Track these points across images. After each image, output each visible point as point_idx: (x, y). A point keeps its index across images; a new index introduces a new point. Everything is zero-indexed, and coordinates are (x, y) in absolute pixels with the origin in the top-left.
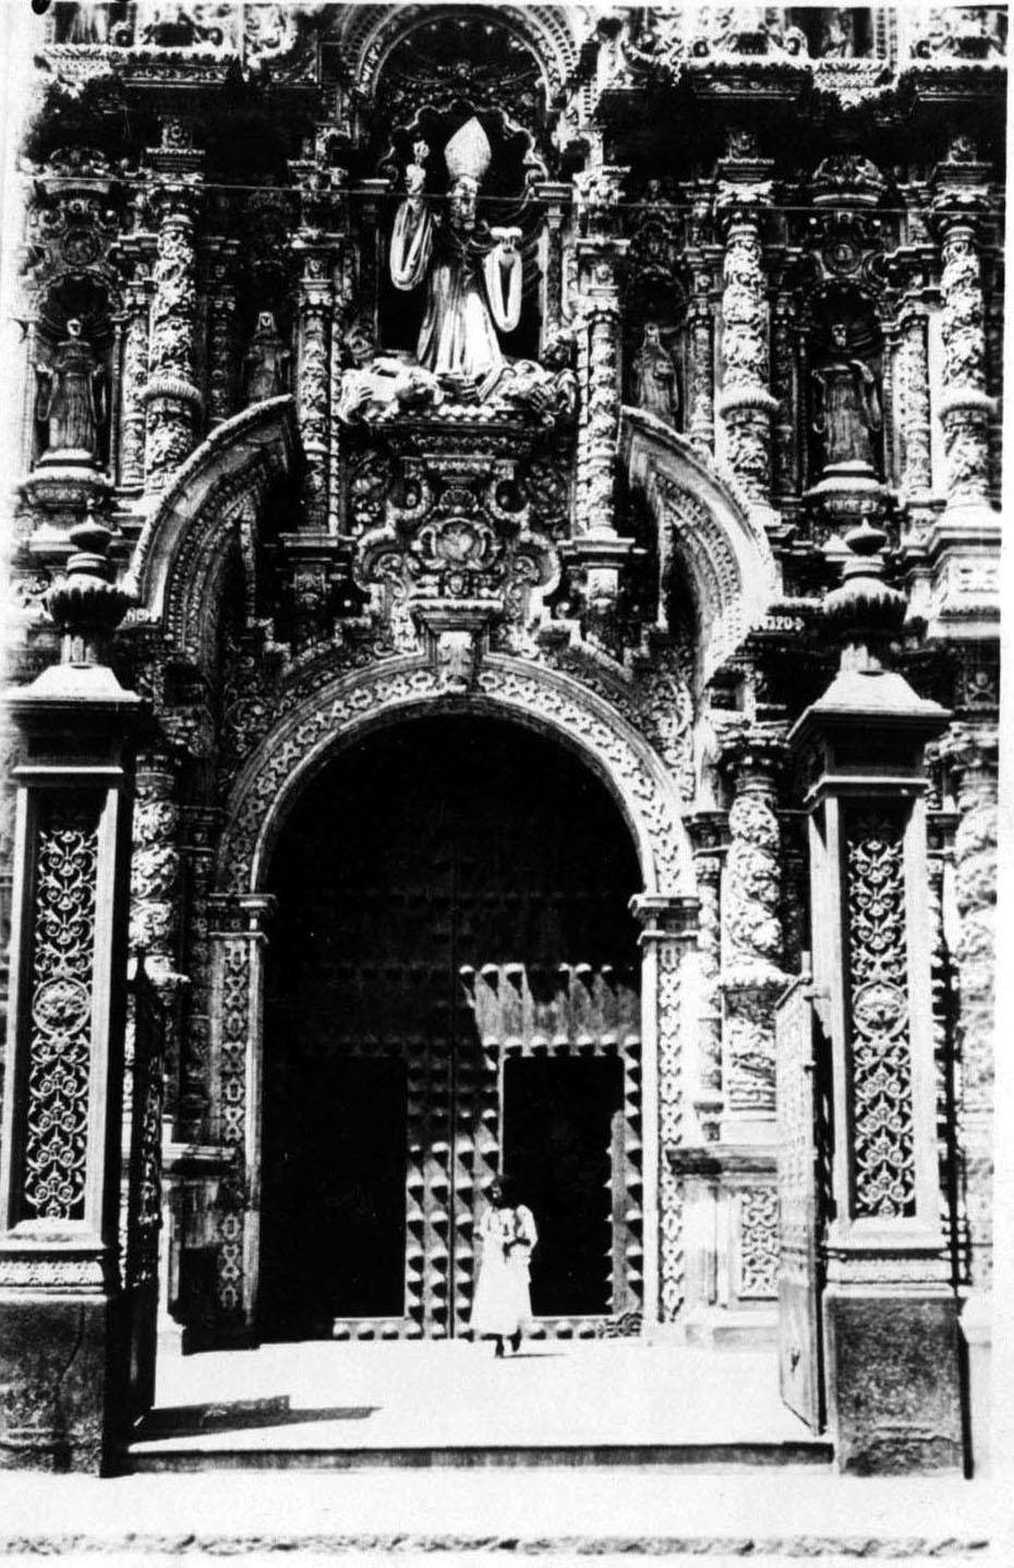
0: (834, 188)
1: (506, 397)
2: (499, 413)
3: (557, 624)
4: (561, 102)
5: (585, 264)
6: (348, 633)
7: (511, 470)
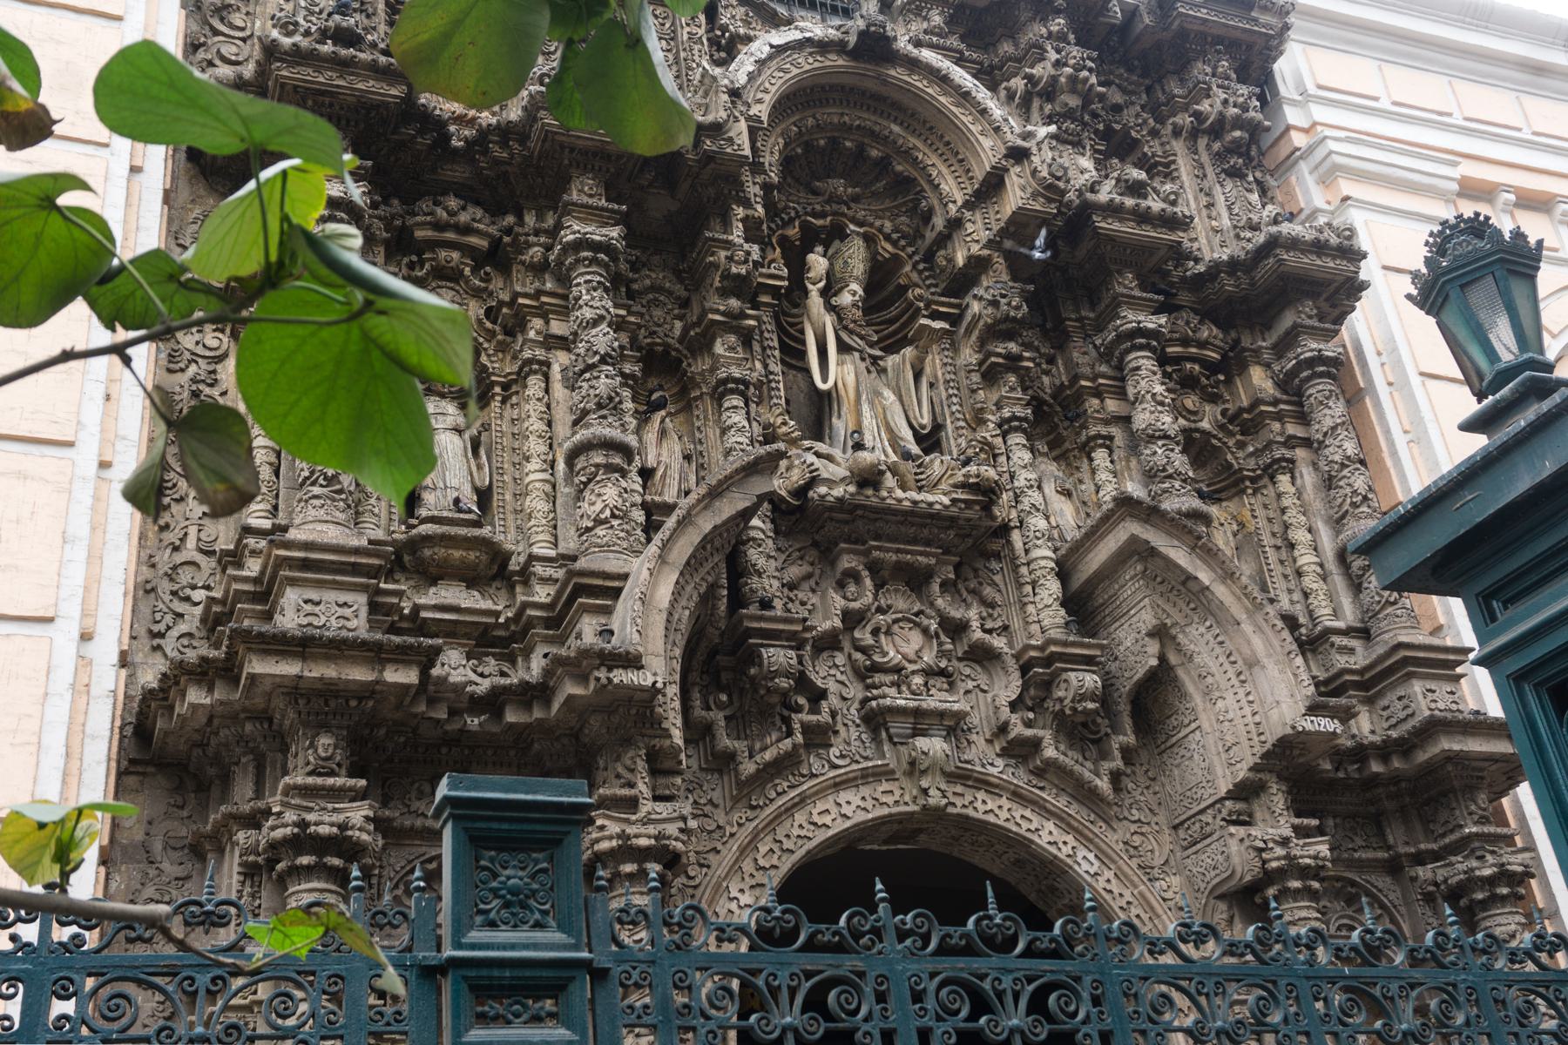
0: (1185, 342)
1: (964, 486)
2: (954, 501)
3: (1029, 732)
4: (956, 224)
5: (990, 376)
6: (807, 729)
7: (951, 568)
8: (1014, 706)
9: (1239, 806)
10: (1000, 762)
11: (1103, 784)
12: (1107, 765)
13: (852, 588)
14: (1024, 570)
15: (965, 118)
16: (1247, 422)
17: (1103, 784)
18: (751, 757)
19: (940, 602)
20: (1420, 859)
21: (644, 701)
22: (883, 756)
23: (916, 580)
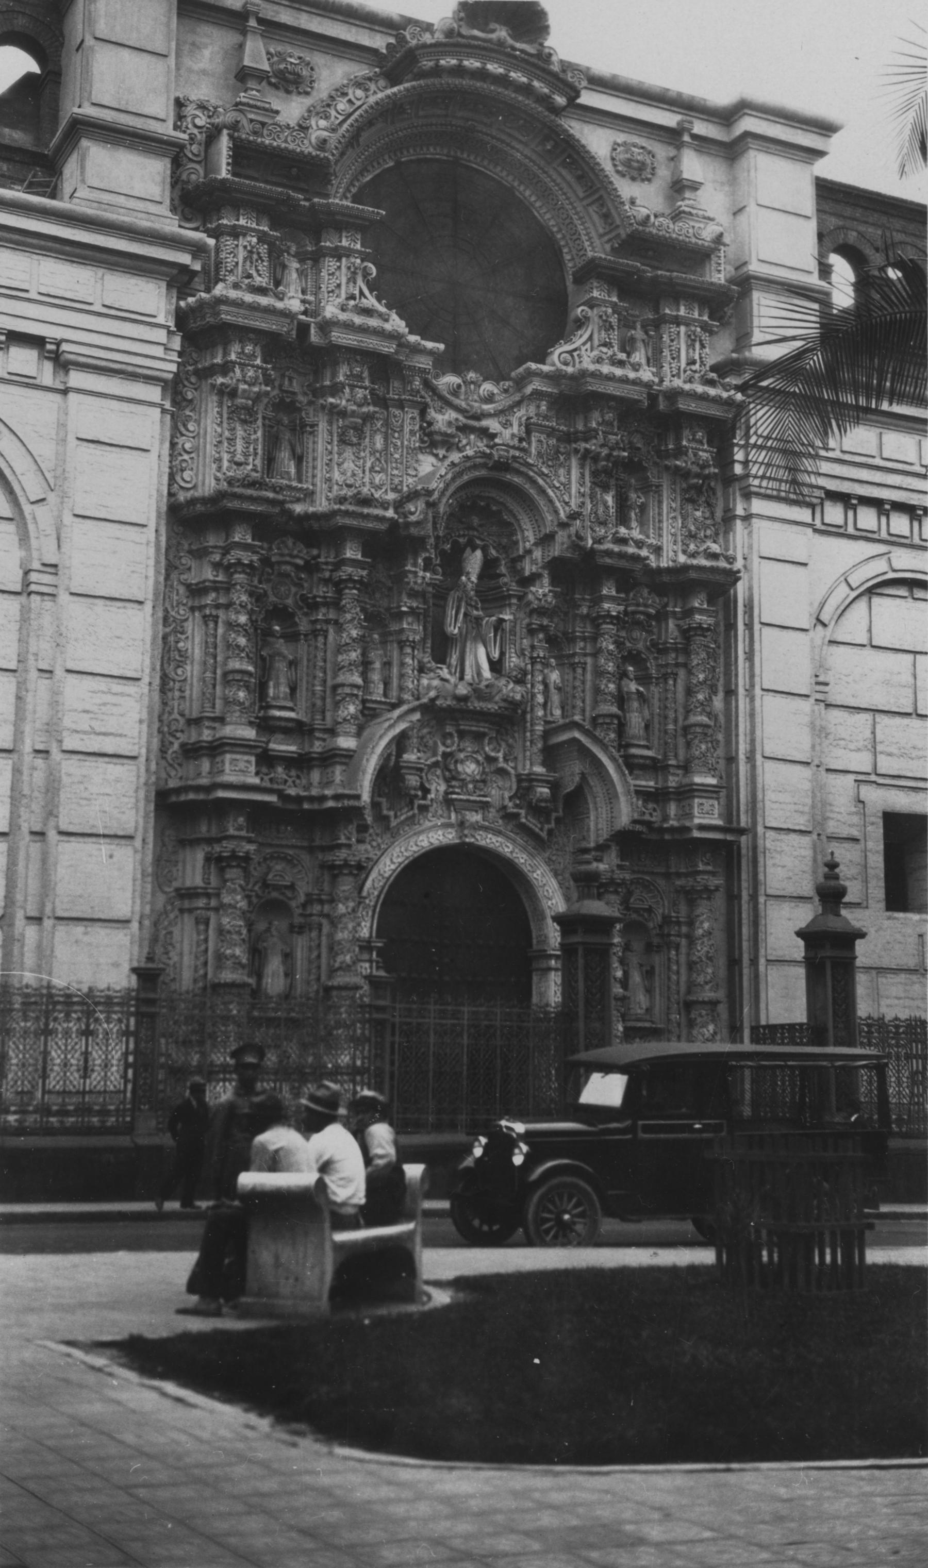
3: (515, 810)
8: (511, 798)
9: (598, 854)
10: (500, 821)
11: (544, 835)
12: (546, 827)
13: (449, 742)
14: (528, 734)
15: (541, 502)
16: (660, 649)
17: (544, 835)
18: (396, 816)
19: (487, 749)
20: (679, 875)
21: (359, 811)
22: (450, 818)
23: (478, 737)
